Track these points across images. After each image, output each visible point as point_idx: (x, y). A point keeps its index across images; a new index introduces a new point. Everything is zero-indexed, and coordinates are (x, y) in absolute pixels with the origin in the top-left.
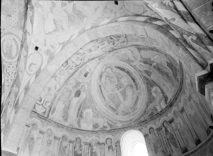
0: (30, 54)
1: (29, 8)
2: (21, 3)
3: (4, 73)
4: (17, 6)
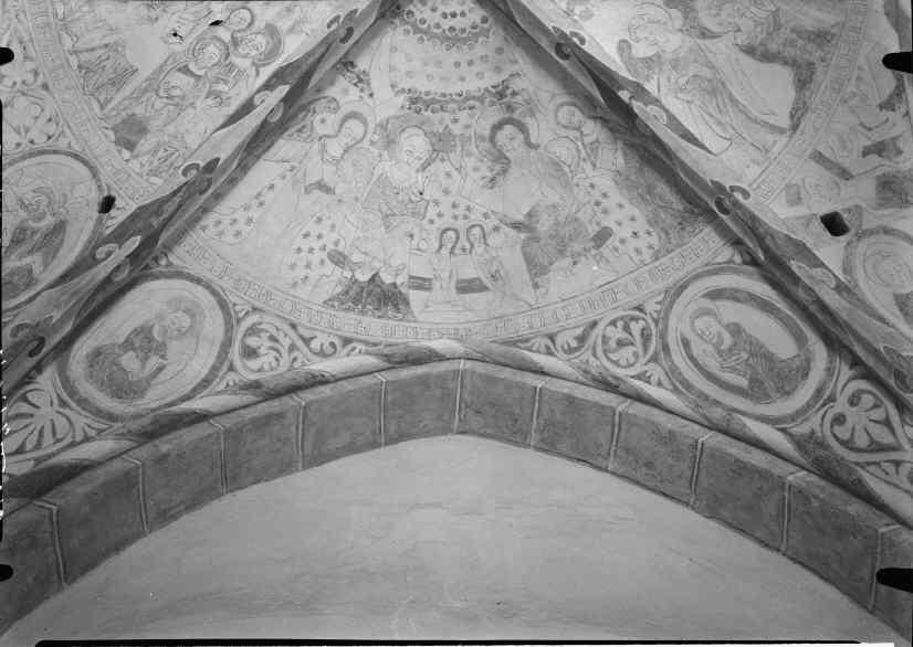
0: (847, 270)
1: (630, 98)
2: (588, 140)
3: (863, 468)
4: (588, 167)
